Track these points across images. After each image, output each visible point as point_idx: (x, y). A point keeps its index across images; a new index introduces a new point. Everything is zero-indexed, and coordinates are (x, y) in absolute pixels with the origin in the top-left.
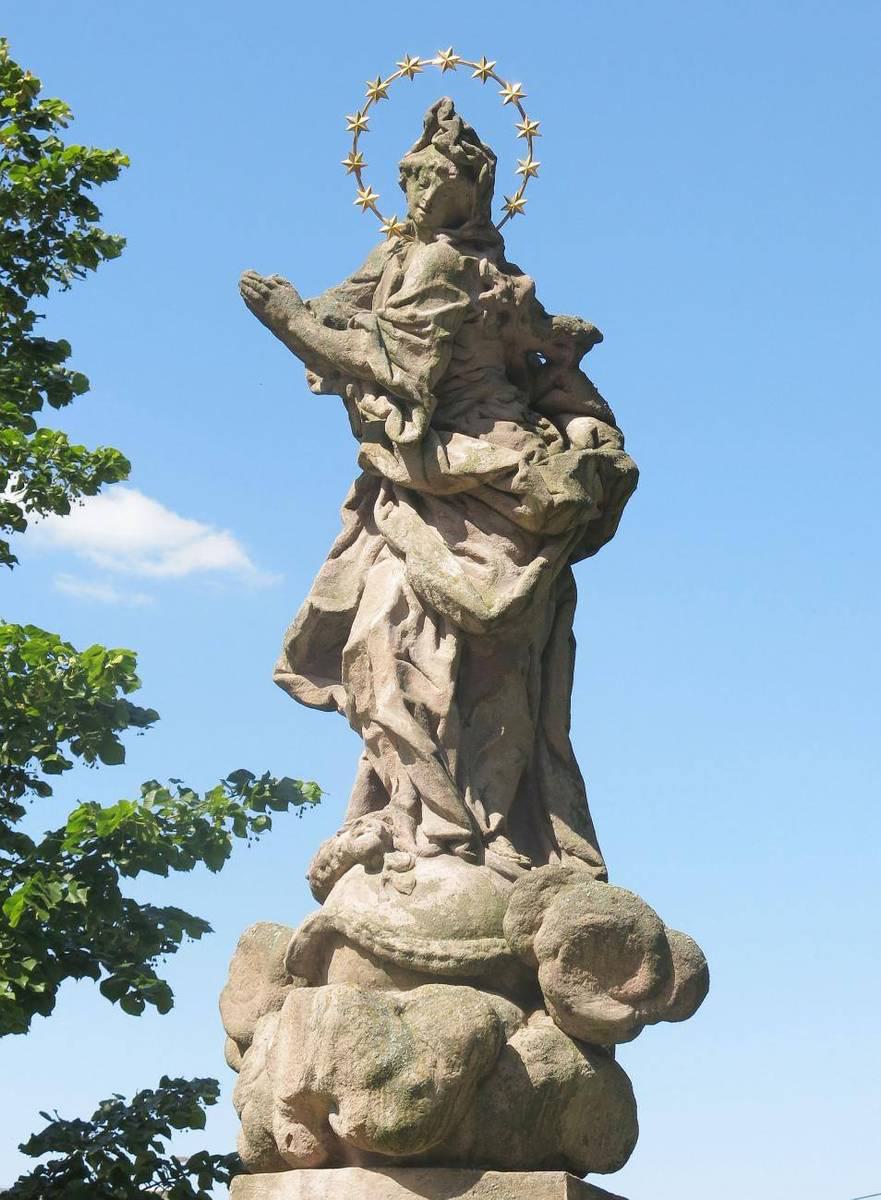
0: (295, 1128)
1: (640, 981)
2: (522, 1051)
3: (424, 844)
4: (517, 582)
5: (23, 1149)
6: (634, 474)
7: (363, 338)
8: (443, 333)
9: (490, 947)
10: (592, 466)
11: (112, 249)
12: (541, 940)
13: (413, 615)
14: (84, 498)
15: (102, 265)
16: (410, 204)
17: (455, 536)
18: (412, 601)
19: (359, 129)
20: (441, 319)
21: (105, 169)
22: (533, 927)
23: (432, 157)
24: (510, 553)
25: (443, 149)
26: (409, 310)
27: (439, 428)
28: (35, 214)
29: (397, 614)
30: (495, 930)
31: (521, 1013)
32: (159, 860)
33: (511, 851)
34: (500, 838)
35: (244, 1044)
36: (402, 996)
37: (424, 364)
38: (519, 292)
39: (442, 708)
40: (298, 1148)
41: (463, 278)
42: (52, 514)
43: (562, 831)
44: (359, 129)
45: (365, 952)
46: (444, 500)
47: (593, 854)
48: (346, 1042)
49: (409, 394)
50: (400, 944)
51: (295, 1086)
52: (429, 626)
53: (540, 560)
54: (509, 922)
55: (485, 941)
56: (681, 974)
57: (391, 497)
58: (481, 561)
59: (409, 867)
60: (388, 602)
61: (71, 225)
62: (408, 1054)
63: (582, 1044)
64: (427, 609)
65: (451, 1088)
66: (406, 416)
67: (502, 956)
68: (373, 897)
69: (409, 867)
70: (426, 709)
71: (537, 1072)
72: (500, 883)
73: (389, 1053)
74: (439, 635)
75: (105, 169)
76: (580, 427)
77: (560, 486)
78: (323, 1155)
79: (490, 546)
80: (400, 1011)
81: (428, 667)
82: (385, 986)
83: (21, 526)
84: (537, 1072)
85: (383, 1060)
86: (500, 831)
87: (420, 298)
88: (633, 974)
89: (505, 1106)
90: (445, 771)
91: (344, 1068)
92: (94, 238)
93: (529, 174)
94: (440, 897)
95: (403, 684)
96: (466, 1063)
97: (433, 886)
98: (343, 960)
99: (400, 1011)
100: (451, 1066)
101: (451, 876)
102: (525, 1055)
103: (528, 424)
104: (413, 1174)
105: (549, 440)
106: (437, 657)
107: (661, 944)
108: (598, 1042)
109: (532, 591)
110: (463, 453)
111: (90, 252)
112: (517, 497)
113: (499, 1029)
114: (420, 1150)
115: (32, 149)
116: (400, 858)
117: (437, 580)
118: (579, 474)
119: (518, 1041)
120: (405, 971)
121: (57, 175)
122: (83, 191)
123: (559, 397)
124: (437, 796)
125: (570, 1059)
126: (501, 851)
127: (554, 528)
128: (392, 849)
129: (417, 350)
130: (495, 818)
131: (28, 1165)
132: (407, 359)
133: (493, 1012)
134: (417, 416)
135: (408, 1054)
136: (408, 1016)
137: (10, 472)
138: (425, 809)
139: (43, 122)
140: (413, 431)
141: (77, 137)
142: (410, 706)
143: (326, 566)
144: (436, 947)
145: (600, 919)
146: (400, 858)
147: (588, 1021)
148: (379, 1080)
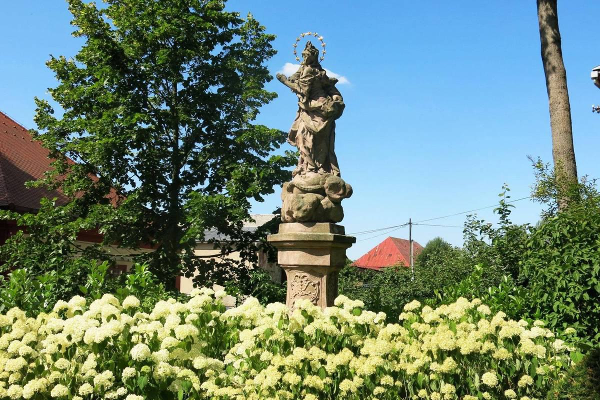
0: (288, 216)
1: (341, 192)
2: (323, 204)
3: (308, 170)
4: (323, 125)
5: (273, 213)
6: (344, 106)
7: (296, 85)
8: (309, 83)
9: (317, 187)
10: (335, 104)
11: (275, 53)
12: (325, 186)
13: (306, 131)
14: (271, 101)
15: (274, 56)
16: (303, 60)
17: (313, 118)
18: (306, 129)
19: (295, 47)
20: (309, 81)
21: (272, 38)
22: (324, 184)
23: (307, 52)
24: (322, 120)
25: (308, 50)
26: (303, 79)
27: (309, 99)
28: (261, 47)
29: (303, 132)
30: (318, 184)
31: (323, 197)
32: (284, 165)
33: (323, 170)
34: (321, 168)
35: (283, 201)
36: (303, 195)
37: (306, 89)
38: (323, 74)
39: (310, 147)
40: (288, 220)
41: (312, 73)
42: (266, 104)
43: (333, 166)
44: (295, 47)
45: (298, 188)
46: (311, 111)
47: (338, 170)
48: (293, 203)
49: (304, 94)
50: (303, 187)
51: (287, 210)
52: (309, 133)
53: (327, 121)
54: (320, 183)
55: (317, 186)
56: (348, 190)
57: (303, 111)
58: (317, 122)
59: (305, 174)
60: (302, 130)
61: (267, 49)
62: (304, 204)
63: (333, 202)
64: (308, 131)
65: (310, 210)
66: (303, 98)
67: (319, 188)
68: (299, 179)
69: (305, 174)
70: (308, 148)
71: (325, 207)
72: (320, 176)
73: (301, 204)
74: (310, 135)
75: (272, 38)
76: (335, 97)
77: (329, 108)
78: (293, 221)
79: (318, 119)
80: (303, 198)
81: (308, 140)
82: (300, 193)
83: (261, 106)
84: (325, 207)
85: (299, 206)
86: (321, 167)
87: (305, 77)
88: (340, 191)
89: (320, 212)
90: (311, 158)
91: (294, 207)
92: (272, 51)
93: (324, 53)
94: (310, 179)
95: (304, 143)
96: (313, 206)
97: (309, 177)
98: (295, 189)
99: (303, 198)
100: (310, 206)
101: (312, 176)
102: (323, 204)
103: (326, 97)
104: (305, 223)
105: (329, 99)
106: (310, 139)
107: (344, 186)
108: (337, 203)
109: (325, 127)
110: (314, 104)
111: (272, 53)
112: (323, 111)
113: (318, 201)
114: (306, 220)
115: (258, 35)
116: (304, 172)
117: (309, 126)
118: (333, 106)
119: (322, 202)
120: (304, 191)
121: (263, 40)
122: (269, 43)
123: (331, 92)
124: (309, 162)
125: (331, 204)
126: (321, 170)
127: (329, 116)
128: (303, 171)
129: (305, 86)
130: (321, 165)
131: (274, 216)
132: (304, 88)
133: (317, 198)
134: (305, 98)
135: (304, 204)
136: (304, 199)
137: (228, 115)
138: (309, 165)
139: (260, 30)
140: (304, 100)
141: (267, 33)
142: (305, 147)
143: (294, 122)
144: (309, 187)
145: (334, 182)
146: (304, 172)
147: (333, 198)
148: (299, 209)
